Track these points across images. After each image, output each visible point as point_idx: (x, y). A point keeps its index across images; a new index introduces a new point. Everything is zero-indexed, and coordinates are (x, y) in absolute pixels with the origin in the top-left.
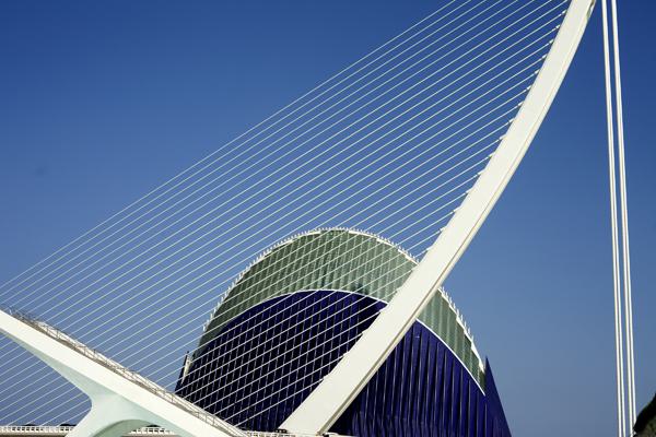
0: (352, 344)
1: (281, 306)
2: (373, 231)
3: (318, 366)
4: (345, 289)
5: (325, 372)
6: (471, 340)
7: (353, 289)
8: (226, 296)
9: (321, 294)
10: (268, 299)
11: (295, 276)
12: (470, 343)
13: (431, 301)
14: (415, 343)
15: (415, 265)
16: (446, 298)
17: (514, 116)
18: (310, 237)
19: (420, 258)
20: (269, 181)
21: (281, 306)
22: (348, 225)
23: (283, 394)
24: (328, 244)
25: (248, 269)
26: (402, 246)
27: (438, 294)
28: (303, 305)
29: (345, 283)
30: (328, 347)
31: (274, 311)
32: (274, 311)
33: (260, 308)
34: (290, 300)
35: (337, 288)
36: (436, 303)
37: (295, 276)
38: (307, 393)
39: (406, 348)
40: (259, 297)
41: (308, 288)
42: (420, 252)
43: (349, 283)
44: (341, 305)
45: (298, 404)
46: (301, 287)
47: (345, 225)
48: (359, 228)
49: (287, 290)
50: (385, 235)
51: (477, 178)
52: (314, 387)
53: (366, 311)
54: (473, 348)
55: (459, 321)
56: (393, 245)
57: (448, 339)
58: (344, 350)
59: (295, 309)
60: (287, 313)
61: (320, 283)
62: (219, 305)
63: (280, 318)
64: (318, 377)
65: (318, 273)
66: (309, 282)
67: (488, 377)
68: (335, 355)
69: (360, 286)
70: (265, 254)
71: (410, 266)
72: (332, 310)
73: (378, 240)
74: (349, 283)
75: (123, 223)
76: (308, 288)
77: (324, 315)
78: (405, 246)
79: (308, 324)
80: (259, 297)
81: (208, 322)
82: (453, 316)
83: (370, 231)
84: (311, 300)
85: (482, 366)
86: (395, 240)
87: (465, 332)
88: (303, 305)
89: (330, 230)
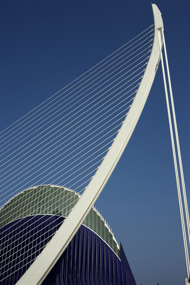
0: (50, 238)
1: (19, 224)
3: (34, 251)
4: (50, 214)
5: (38, 254)
6: (113, 234)
7: (54, 213)
10: (12, 221)
11: (40, 204)
12: (112, 236)
13: (88, 215)
16: (99, 215)
17: (120, 128)
18: (29, 191)
19: (81, 193)
21: (19, 224)
24: (40, 194)
28: (29, 223)
29: (50, 211)
30: (39, 241)
31: (15, 227)
32: (15, 227)
33: (8, 226)
34: (23, 221)
35: (46, 213)
36: (91, 215)
37: (40, 204)
38: (29, 266)
39: (81, 234)
40: (8, 221)
41: (32, 214)
42: (81, 190)
43: (52, 211)
44: (48, 222)
46: (39, 213)
49: (21, 216)
50: (67, 186)
51: (102, 161)
52: (32, 262)
53: (59, 221)
54: (114, 238)
55: (106, 225)
56: (72, 191)
58: (46, 242)
59: (25, 226)
60: (22, 228)
61: (37, 212)
63: (18, 231)
64: (34, 257)
65: (36, 206)
66: (43, 210)
67: (122, 252)
68: (42, 245)
69: (57, 211)
70: (11, 200)
72: (37, 224)
73: (51, 186)
74: (52, 211)
76: (42, 213)
77: (40, 228)
79: (32, 233)
80: (8, 221)
82: (103, 223)
83: (59, 185)
84: (33, 220)
85: (118, 247)
87: (109, 231)
88: (29, 223)
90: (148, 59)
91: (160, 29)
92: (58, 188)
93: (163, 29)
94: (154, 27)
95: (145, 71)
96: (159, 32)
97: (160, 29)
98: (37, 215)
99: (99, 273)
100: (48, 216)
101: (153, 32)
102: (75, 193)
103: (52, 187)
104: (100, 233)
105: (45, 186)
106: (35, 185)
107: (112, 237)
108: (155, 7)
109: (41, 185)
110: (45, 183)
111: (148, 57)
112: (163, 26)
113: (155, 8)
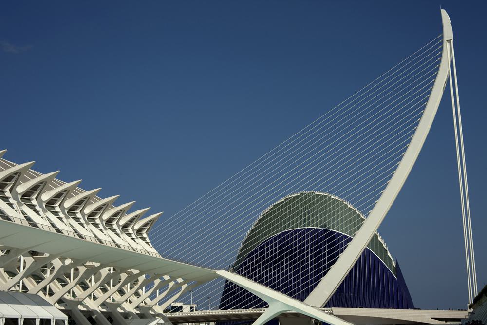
2: (331, 193)
4: (301, 227)
6: (387, 249)
7: (321, 226)
8: (249, 233)
9: (308, 230)
14: (366, 259)
15: (364, 220)
19: (367, 216)
20: (344, 138)
22: (317, 190)
23: (303, 287)
24: (305, 201)
25: (256, 222)
26: (346, 200)
27: (375, 237)
38: (316, 285)
45: (311, 290)
47: (315, 190)
48: (323, 191)
52: (319, 282)
54: (389, 254)
56: (340, 200)
57: (375, 250)
62: (245, 238)
65: (301, 217)
67: (397, 269)
71: (363, 220)
73: (332, 197)
75: (319, 137)
78: (346, 200)
81: (240, 248)
85: (394, 263)
86: (342, 197)
87: (384, 245)
89: (308, 192)
90: (434, 83)
91: (449, 41)
92: (320, 195)
93: (452, 41)
94: (442, 37)
95: (432, 88)
96: (448, 45)
97: (449, 41)
98: (307, 228)
99: (373, 292)
100: (317, 230)
101: (442, 43)
102: (344, 202)
103: (333, 199)
104: (373, 248)
105: (305, 194)
106: (295, 192)
107: (387, 253)
108: (444, 12)
109: (302, 192)
110: (307, 190)
111: (433, 80)
112: (453, 39)
113: (444, 14)
